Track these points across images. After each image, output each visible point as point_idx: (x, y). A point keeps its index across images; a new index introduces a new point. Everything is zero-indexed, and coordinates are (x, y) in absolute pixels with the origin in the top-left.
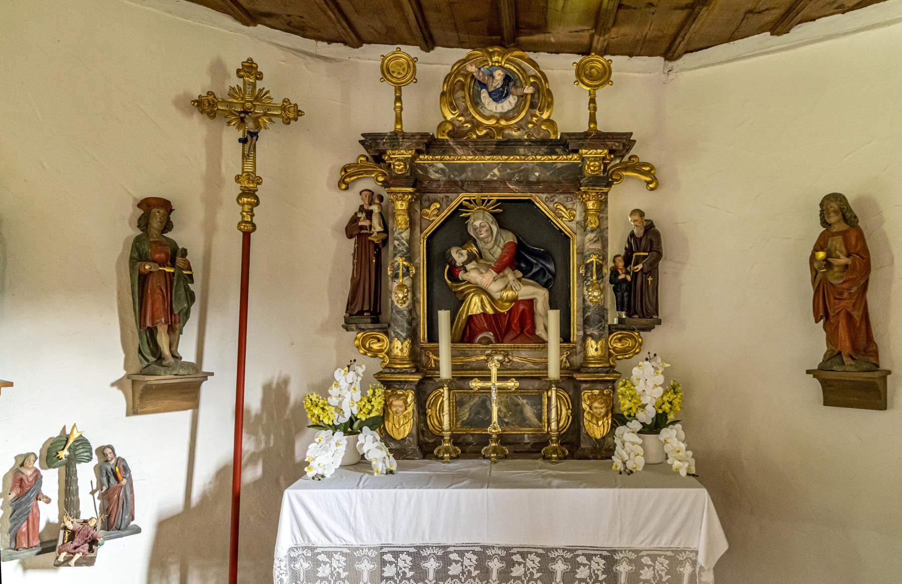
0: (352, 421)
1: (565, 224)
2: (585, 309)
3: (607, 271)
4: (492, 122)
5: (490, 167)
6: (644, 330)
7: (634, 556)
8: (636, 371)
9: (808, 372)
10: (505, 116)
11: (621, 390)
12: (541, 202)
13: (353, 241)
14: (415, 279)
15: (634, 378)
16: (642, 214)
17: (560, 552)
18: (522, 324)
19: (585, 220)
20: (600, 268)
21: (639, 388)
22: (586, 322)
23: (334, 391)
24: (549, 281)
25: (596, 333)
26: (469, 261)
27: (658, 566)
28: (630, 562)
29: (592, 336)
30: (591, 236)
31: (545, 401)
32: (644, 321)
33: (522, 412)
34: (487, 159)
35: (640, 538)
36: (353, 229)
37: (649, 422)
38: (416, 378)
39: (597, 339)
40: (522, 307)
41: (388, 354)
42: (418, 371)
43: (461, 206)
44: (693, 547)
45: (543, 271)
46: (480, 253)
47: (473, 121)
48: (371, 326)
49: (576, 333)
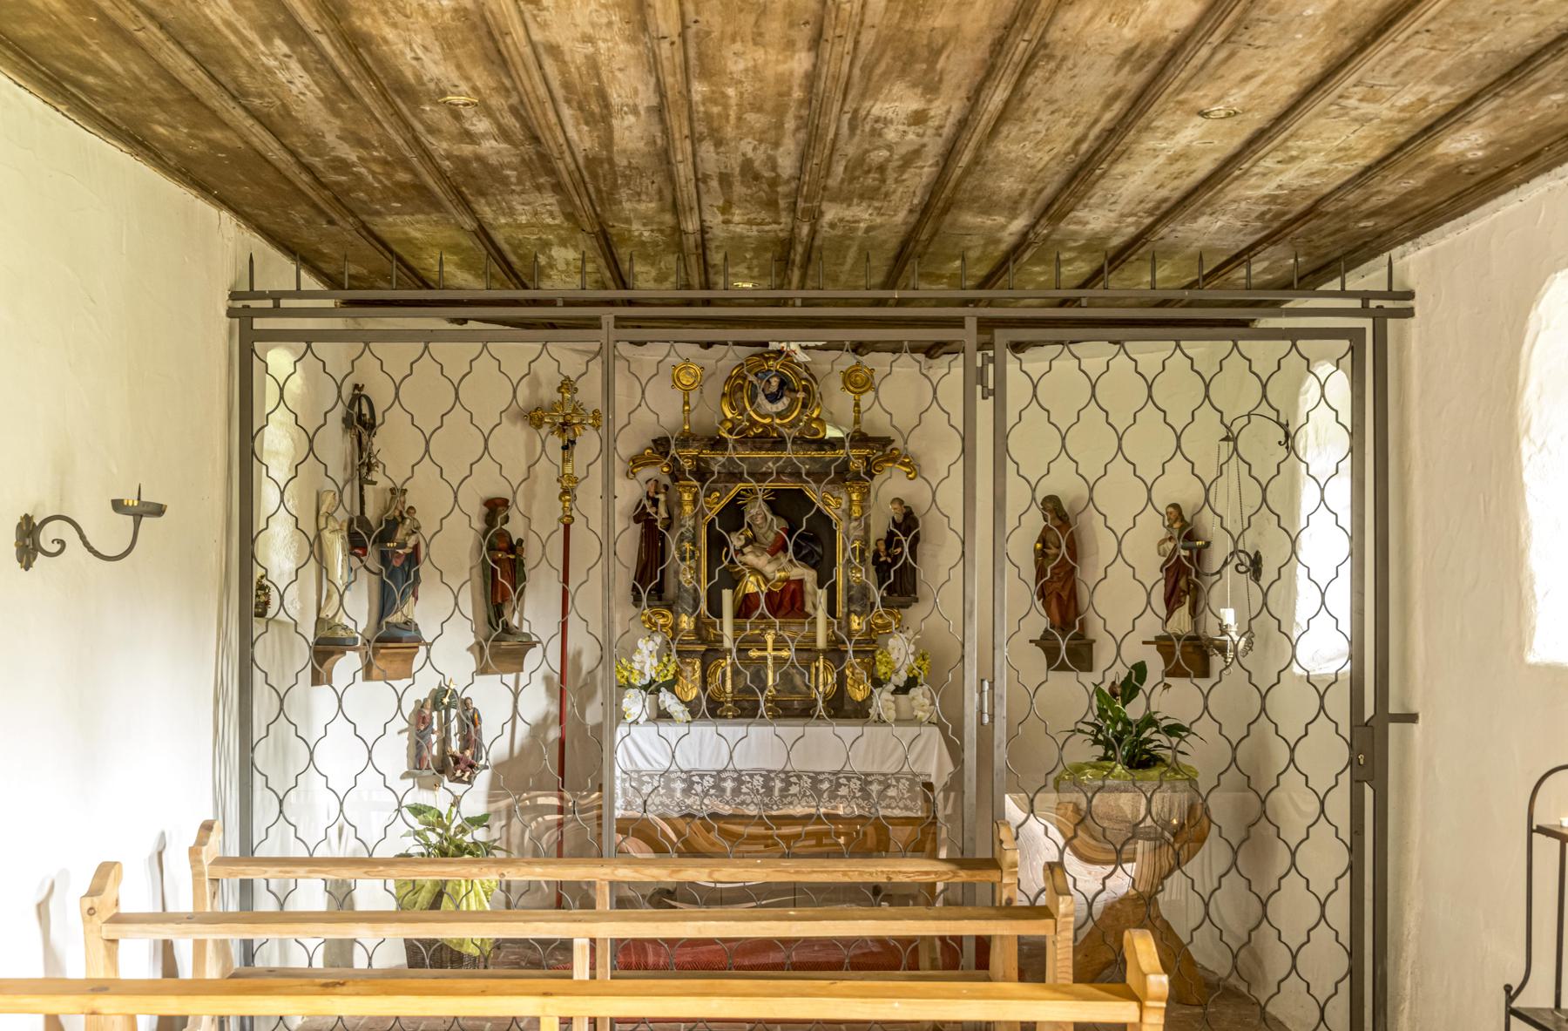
0: (652, 681)
1: (831, 512)
2: (849, 588)
3: (869, 555)
4: (767, 421)
5: (765, 461)
6: (902, 607)
7: (882, 778)
8: (891, 642)
9: (1031, 641)
10: (780, 415)
11: (879, 657)
12: (813, 492)
13: (640, 526)
14: (698, 562)
15: (889, 648)
16: (901, 502)
17: (827, 775)
18: (793, 604)
19: (850, 509)
20: (862, 552)
21: (894, 657)
22: (850, 600)
23: (637, 657)
24: (817, 562)
25: (858, 609)
26: (746, 545)
27: (901, 786)
28: (880, 783)
29: (855, 613)
30: (854, 524)
31: (813, 671)
32: (902, 599)
33: (792, 680)
34: (763, 454)
35: (888, 764)
36: (641, 516)
37: (902, 685)
38: (703, 648)
39: (859, 615)
40: (793, 586)
41: (672, 628)
42: (703, 641)
43: (738, 494)
44: (928, 772)
45: (812, 553)
46: (754, 536)
47: (750, 419)
48: (658, 603)
49: (841, 609)
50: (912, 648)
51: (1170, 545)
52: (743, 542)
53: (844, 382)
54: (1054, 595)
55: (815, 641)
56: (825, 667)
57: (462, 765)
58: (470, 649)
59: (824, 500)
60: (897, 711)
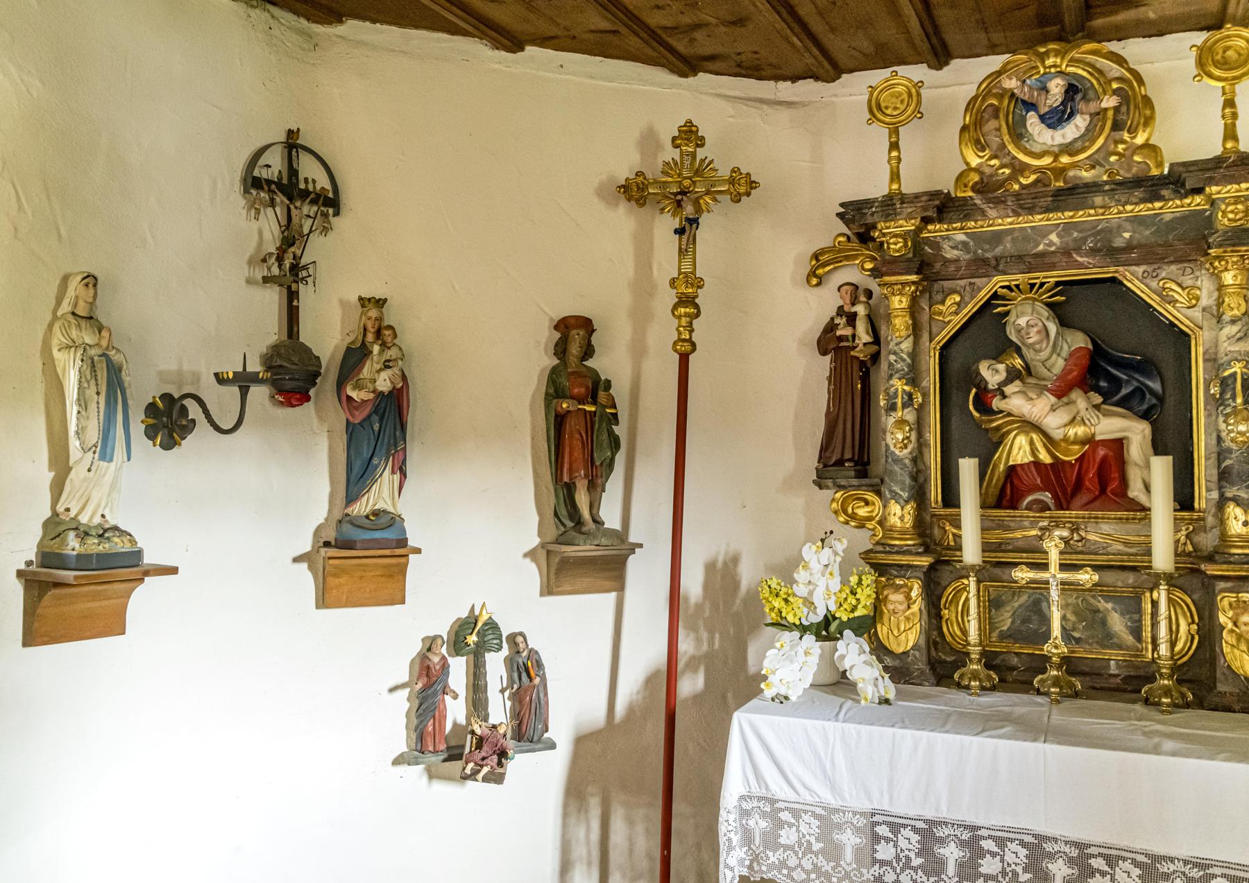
0: (828, 620)
1: (1179, 313)
2: (1222, 454)
4: (1047, 161)
5: (1042, 232)
10: (1069, 149)
14: (921, 411)
17: (1179, 866)
18: (1103, 484)
19: (1220, 303)
22: (1224, 476)
23: (801, 575)
29: (1237, 501)
31: (1148, 607)
33: (1104, 622)
34: (1038, 220)
38: (925, 561)
40: (1101, 452)
43: (995, 296)
45: (1140, 392)
46: (1028, 368)
48: (855, 482)
49: (1204, 496)
52: (1002, 376)
55: (1148, 553)
56: (1170, 601)
57: (486, 750)
58: (531, 554)
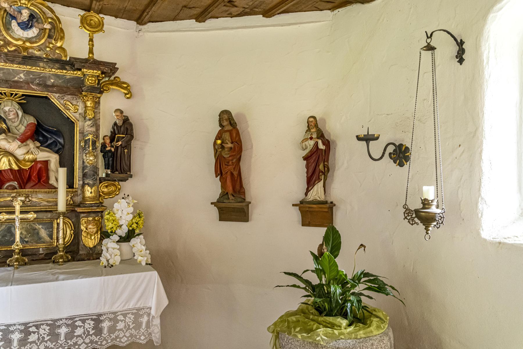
1: (71, 114)
2: (84, 168)
3: (99, 145)
4: (20, 43)
5: (18, 73)
6: (122, 181)
7: (113, 316)
8: (116, 205)
10: (29, 40)
11: (106, 217)
15: (115, 210)
16: (122, 112)
17: (64, 321)
20: (94, 143)
21: (118, 216)
24: (60, 149)
25: (91, 182)
29: (88, 184)
31: (55, 226)
32: (122, 175)
33: (38, 233)
34: (15, 67)
35: (117, 305)
37: (124, 235)
39: (91, 186)
40: (39, 165)
44: (148, 305)
45: (55, 143)
46: (8, 129)
49: (77, 183)
50: (131, 209)
51: (312, 143)
53: (82, 22)
54: (229, 173)
55: (56, 205)
59: (65, 105)
60: (121, 255)
